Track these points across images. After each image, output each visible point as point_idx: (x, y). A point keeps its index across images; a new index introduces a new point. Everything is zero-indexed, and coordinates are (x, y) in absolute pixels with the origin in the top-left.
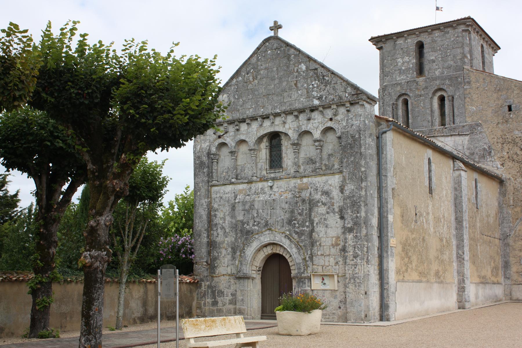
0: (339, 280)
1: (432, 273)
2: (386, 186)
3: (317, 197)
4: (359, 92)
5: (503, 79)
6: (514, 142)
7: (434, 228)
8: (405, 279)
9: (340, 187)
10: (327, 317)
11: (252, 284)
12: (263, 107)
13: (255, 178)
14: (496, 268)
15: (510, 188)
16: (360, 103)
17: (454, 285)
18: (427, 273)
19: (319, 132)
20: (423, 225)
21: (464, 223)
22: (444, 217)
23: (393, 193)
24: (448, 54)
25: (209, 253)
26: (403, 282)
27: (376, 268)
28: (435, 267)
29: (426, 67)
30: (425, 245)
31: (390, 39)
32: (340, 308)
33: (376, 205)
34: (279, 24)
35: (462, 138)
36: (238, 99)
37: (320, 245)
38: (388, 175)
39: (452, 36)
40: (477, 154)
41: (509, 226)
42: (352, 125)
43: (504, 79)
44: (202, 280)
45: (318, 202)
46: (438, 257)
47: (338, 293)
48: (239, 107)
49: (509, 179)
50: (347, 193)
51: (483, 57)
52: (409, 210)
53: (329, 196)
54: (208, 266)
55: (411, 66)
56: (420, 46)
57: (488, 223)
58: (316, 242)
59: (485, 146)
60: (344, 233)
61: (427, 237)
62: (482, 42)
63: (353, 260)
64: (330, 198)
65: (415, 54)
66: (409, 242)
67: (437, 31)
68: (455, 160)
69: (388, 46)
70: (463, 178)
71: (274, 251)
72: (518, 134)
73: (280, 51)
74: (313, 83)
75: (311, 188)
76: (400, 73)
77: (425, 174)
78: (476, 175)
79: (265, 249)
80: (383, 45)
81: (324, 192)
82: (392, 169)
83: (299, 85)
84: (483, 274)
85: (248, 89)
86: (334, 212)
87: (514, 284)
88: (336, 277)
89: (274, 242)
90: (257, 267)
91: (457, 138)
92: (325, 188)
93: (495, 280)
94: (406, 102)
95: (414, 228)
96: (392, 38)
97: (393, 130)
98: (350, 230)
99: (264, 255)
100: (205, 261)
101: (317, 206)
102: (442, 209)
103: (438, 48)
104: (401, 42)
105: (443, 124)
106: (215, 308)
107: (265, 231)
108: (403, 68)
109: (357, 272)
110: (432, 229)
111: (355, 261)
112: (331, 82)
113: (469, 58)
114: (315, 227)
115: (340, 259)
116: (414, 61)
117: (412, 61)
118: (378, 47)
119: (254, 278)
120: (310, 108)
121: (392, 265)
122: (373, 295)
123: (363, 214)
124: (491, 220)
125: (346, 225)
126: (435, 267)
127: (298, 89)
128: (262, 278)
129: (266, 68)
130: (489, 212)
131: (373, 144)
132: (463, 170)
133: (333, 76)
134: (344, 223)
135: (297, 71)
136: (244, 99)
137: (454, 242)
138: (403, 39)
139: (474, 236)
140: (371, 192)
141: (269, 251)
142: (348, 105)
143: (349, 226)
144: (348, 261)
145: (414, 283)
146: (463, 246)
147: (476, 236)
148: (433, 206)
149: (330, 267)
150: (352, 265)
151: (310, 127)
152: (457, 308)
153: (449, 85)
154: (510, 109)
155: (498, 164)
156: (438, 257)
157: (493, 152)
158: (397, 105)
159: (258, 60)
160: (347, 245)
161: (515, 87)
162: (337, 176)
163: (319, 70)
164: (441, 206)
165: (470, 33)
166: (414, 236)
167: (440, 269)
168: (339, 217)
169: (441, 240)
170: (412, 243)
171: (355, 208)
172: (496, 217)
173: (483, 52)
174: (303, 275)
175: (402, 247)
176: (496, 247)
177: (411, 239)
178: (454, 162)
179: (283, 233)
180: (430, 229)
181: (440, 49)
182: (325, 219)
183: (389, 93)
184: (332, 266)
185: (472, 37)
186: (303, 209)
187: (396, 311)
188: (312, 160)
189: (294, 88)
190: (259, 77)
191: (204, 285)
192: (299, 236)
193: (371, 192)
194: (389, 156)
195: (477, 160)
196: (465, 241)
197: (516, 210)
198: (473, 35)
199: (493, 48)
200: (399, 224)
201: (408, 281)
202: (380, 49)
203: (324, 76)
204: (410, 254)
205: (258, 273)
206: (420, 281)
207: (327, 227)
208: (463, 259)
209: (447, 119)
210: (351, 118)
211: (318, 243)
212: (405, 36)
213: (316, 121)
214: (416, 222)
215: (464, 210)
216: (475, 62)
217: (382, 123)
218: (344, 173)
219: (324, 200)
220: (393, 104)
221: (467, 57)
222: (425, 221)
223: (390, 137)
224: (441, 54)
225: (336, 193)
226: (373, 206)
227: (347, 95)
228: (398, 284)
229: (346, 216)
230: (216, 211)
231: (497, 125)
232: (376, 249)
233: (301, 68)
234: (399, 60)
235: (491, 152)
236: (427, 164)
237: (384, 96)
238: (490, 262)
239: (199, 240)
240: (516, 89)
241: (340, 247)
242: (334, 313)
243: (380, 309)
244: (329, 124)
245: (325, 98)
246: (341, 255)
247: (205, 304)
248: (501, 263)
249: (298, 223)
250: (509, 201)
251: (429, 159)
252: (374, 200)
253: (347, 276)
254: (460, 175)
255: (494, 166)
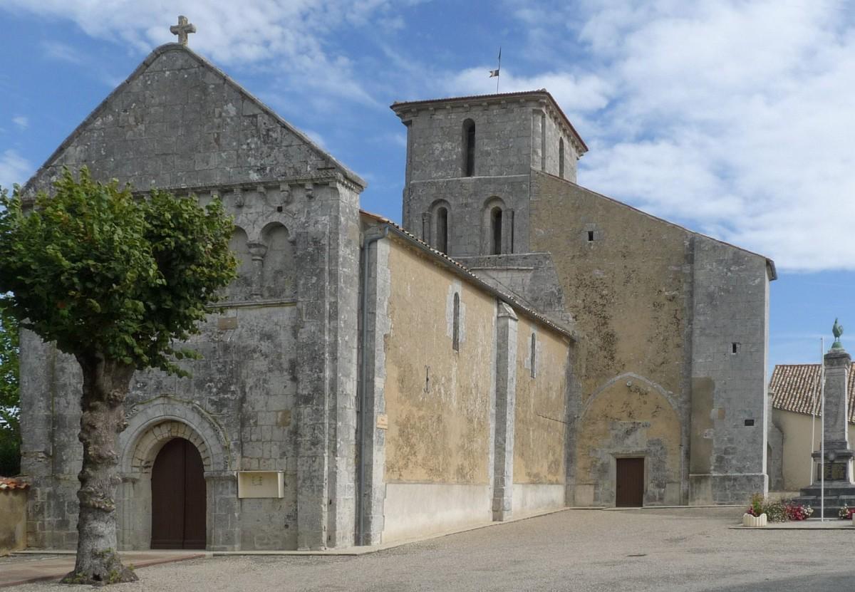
0: (287, 482)
1: (452, 469)
2: (374, 331)
3: (253, 342)
4: (330, 166)
5: (584, 192)
6: (593, 286)
7: (458, 403)
8: (404, 479)
9: (293, 327)
10: (266, 541)
11: (132, 491)
12: (156, 176)
13: (792, 488)
14: (556, 462)
15: (583, 352)
16: (331, 185)
17: (487, 487)
18: (443, 469)
19: (258, 230)
20: (440, 397)
21: (509, 398)
22: (477, 386)
23: (385, 342)
24: (510, 145)
25: (51, 437)
26: (399, 483)
27: (352, 461)
28: (457, 460)
29: (478, 162)
30: (441, 428)
31: (423, 110)
32: (287, 526)
33: (355, 361)
34: (189, 23)
35: (522, 274)
36: (106, 156)
37: (256, 423)
38: (378, 312)
39: (518, 118)
40: (541, 299)
41: (578, 404)
42: (317, 222)
43: (587, 193)
44: (37, 484)
45: (254, 351)
46: (463, 447)
47: (284, 504)
48: (108, 173)
49: (583, 338)
50: (303, 336)
51: (562, 157)
52: (414, 372)
53: (272, 341)
54: (50, 460)
55: (455, 157)
56: (470, 129)
57: (548, 399)
58: (249, 419)
59: (553, 289)
60: (296, 405)
61: (445, 415)
62: (561, 134)
63: (311, 449)
64: (276, 346)
65: (461, 138)
66: (412, 422)
67: (496, 107)
68: (501, 302)
69: (421, 122)
70: (510, 331)
71: (174, 434)
72: (599, 275)
73: (189, 74)
74: (249, 141)
75: (243, 327)
76: (437, 167)
77: (447, 318)
78: (532, 330)
79: (157, 431)
80: (413, 119)
81: (265, 335)
82: (386, 303)
83: (223, 142)
84: (535, 471)
85: (125, 141)
86: (281, 370)
87: (579, 484)
88: (280, 476)
89: (173, 417)
90: (142, 460)
91: (516, 275)
92: (267, 329)
93: (554, 479)
94: (443, 215)
95: (423, 401)
96: (427, 109)
97: (391, 241)
98: (307, 400)
99: (156, 441)
100: (43, 450)
101: (252, 358)
102: (474, 374)
103: (497, 134)
104: (440, 117)
105: (497, 251)
106: (64, 533)
107: (156, 399)
108: (442, 159)
109: (317, 467)
110: (455, 404)
111: (314, 450)
112: (281, 142)
113: (540, 155)
114: (248, 394)
115: (290, 448)
116: (460, 150)
117: (455, 149)
118: (404, 121)
119: (137, 480)
120: (241, 184)
121: (380, 458)
122: (342, 504)
123: (328, 373)
124: (554, 395)
125: (300, 391)
126: (457, 460)
127: (221, 149)
128: (155, 481)
129: (160, 105)
130: (551, 383)
131: (355, 259)
132: (512, 318)
133: (285, 131)
134: (297, 388)
135: (220, 116)
136: (118, 157)
137: (492, 425)
138: (445, 112)
139: (525, 417)
140: (347, 338)
141: (164, 434)
142: (309, 186)
143: (305, 392)
144: (301, 450)
145: (419, 485)
146: (505, 431)
147: (528, 417)
148: (459, 368)
149: (271, 461)
150: (308, 457)
151: (241, 220)
152: (491, 519)
153: (509, 193)
154: (591, 238)
155: (570, 315)
156: (463, 447)
157: (563, 298)
158: (430, 217)
159: (146, 87)
160: (301, 424)
161: (601, 205)
162: (288, 309)
163: (259, 118)
164: (473, 370)
165: (543, 117)
166: (421, 413)
167: (466, 464)
168: (289, 377)
169: (470, 421)
170: (418, 424)
171: (316, 364)
172: (561, 392)
173: (561, 149)
174: (223, 474)
175: (400, 430)
176: (558, 434)
177: (416, 416)
178: (498, 304)
179: (188, 403)
180: (451, 402)
181: (499, 135)
182: (265, 381)
183: (419, 196)
184: (275, 459)
185: (547, 123)
186: (226, 362)
187: (383, 529)
188: (245, 279)
189: (214, 147)
190: (147, 119)
191: (41, 493)
192: (217, 408)
193: (347, 338)
194: (380, 281)
195: (541, 308)
196: (508, 423)
197: (588, 382)
198: (549, 121)
199: (577, 147)
200: (395, 392)
201: (409, 482)
202: (408, 124)
203: (268, 130)
204: (413, 440)
205: (144, 471)
206: (431, 482)
207: (268, 394)
208: (504, 449)
209: (503, 245)
210: (315, 211)
211: (251, 421)
212: (448, 107)
213: (252, 210)
214: (427, 391)
215: (509, 378)
216: (548, 163)
217: (372, 225)
218: (299, 305)
219: (264, 349)
220: (424, 214)
221: (537, 154)
222: (442, 391)
223: (383, 249)
224: (500, 144)
225: (284, 337)
226: (350, 361)
227: (309, 169)
228: (390, 487)
229: (300, 376)
230: (63, 361)
231: (572, 259)
232: (353, 432)
233: (227, 112)
234: (437, 145)
235: (561, 298)
236: (452, 302)
237: (410, 200)
238: (547, 454)
239: (31, 413)
240: (601, 208)
241: (291, 427)
242: (276, 536)
243: (356, 527)
244: (276, 218)
245: (270, 171)
246: (290, 441)
247: (42, 527)
248: (563, 456)
249: (216, 387)
250: (580, 369)
251: (456, 295)
252: (351, 352)
253: (300, 475)
254: (507, 325)
255: (565, 318)
